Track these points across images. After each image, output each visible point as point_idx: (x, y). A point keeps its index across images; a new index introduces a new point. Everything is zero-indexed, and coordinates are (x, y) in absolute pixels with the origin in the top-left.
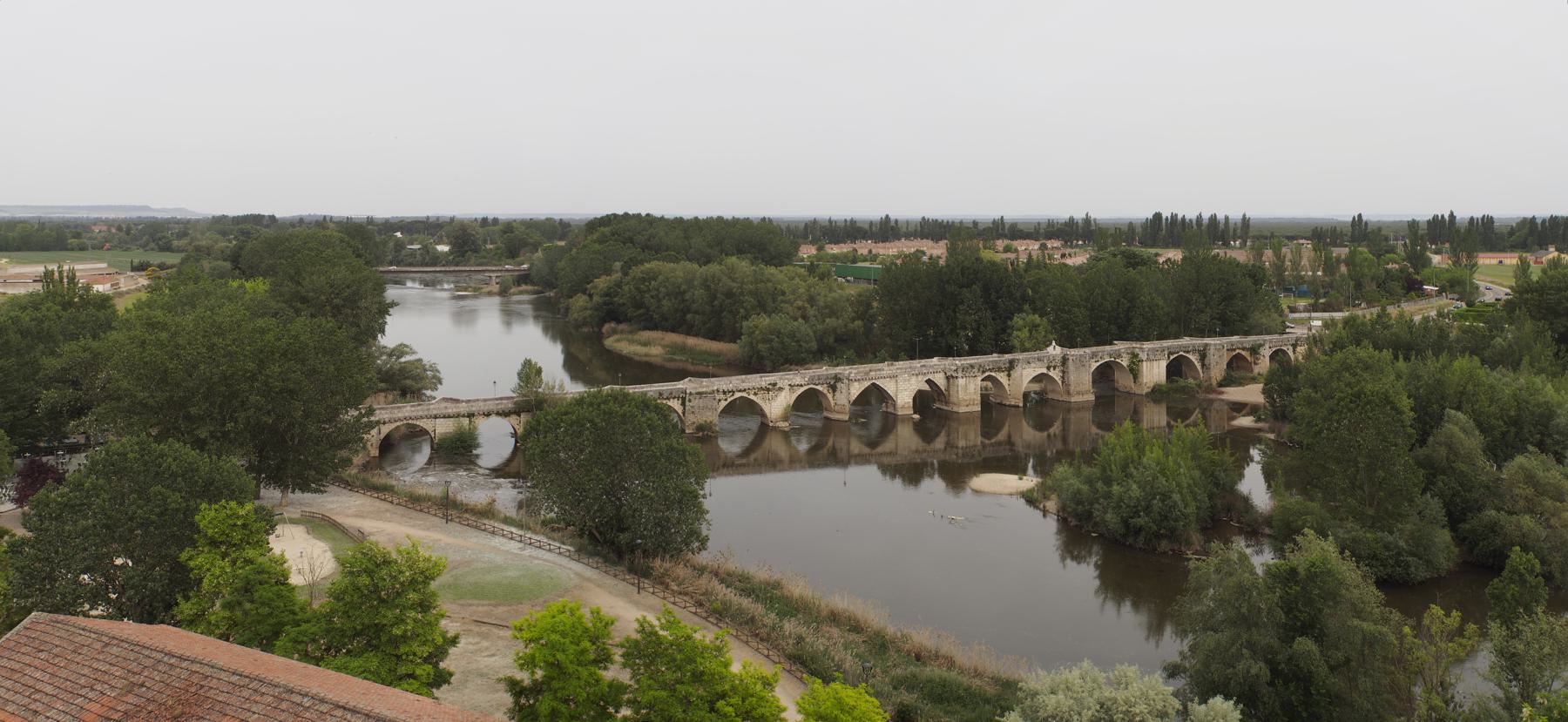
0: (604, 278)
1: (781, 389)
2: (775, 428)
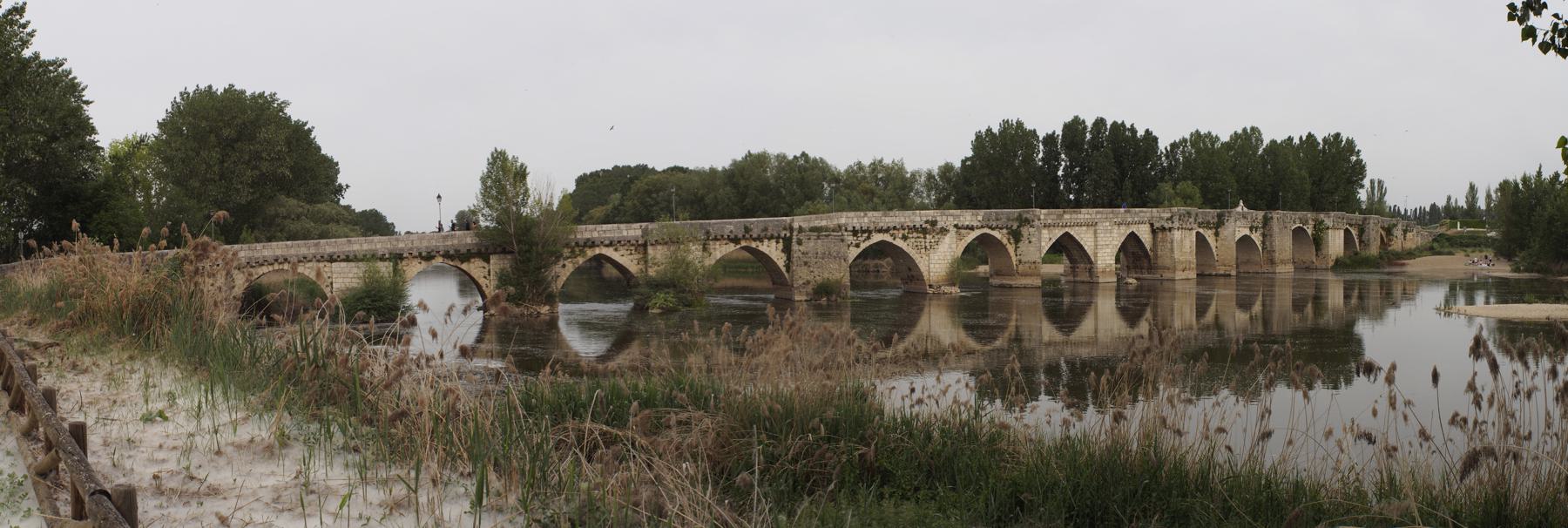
0: (600, 208)
1: (944, 231)
2: (938, 295)
